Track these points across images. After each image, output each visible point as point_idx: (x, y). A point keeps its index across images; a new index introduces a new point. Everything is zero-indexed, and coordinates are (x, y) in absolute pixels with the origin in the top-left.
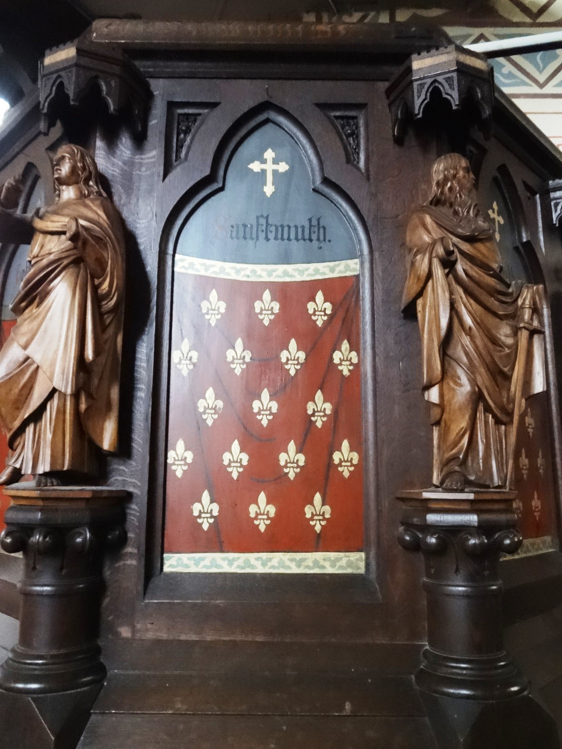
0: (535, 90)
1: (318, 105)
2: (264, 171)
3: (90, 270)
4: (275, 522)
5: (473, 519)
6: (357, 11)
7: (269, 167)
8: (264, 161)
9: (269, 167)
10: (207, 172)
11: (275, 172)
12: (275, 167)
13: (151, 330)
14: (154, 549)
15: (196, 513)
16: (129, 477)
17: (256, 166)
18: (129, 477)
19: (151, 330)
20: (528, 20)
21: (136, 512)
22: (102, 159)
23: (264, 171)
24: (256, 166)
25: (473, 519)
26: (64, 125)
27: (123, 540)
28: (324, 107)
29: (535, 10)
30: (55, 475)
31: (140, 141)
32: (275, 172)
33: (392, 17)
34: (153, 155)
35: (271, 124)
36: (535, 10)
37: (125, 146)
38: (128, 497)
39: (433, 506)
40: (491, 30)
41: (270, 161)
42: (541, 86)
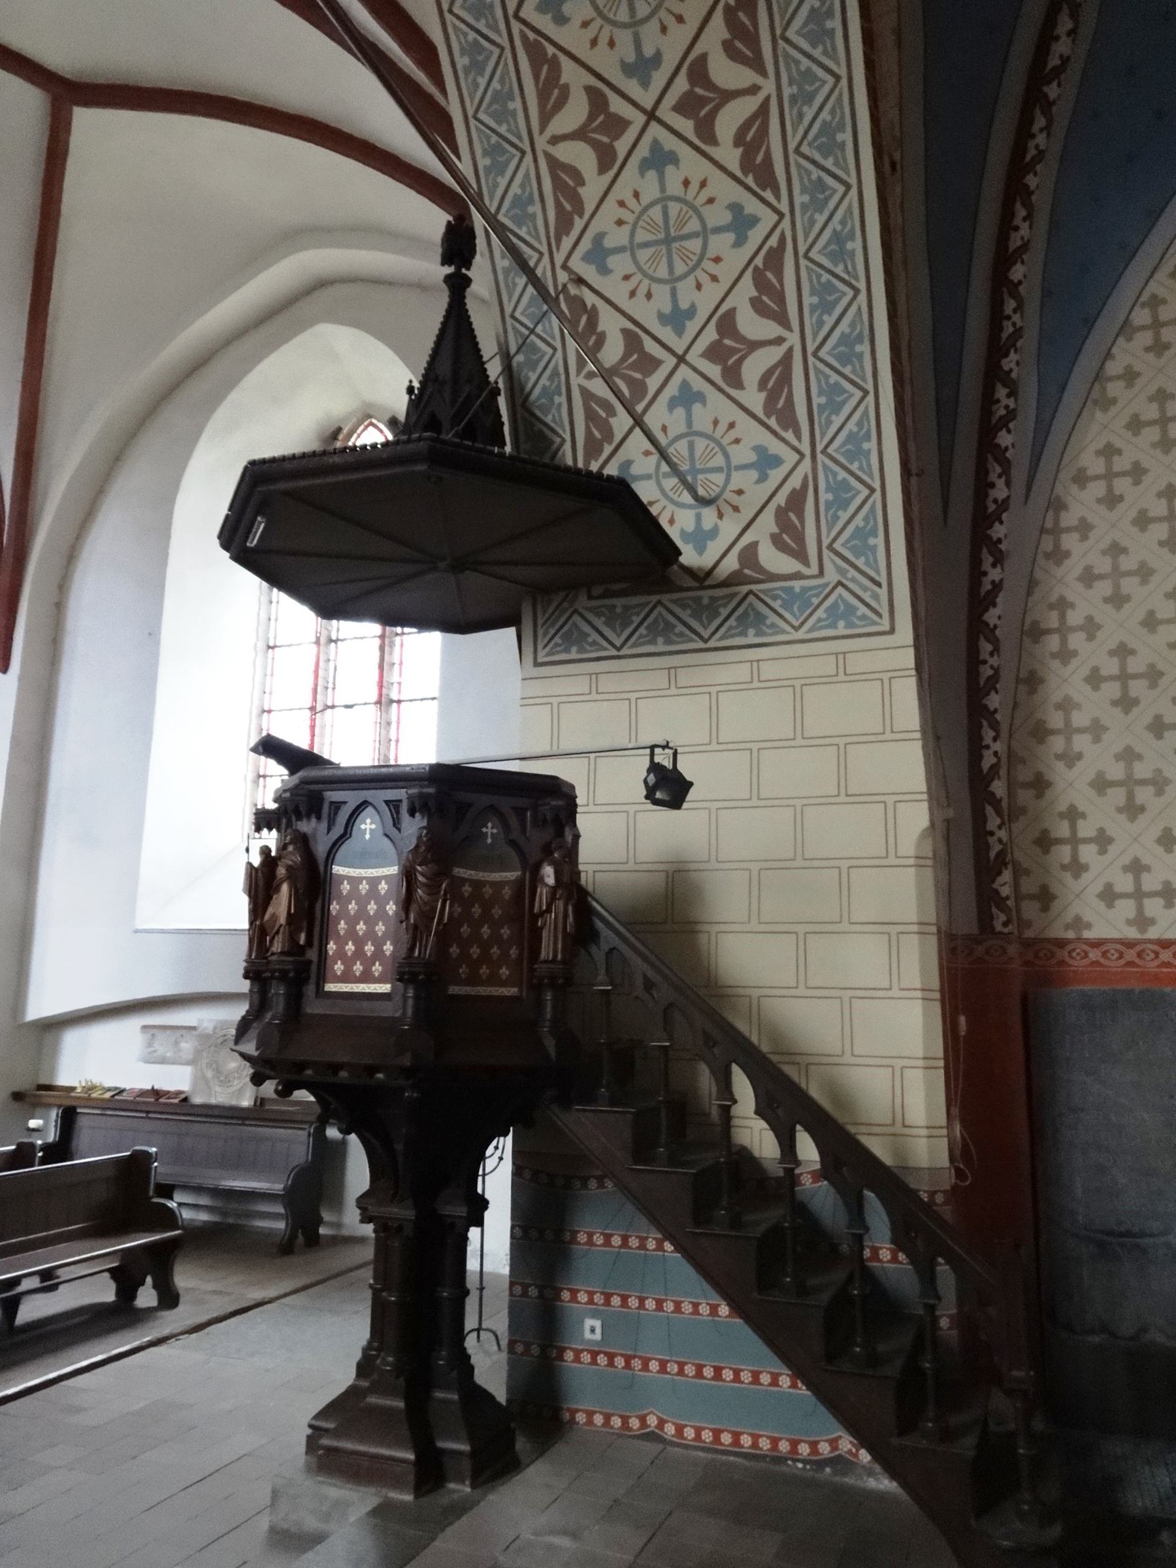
0: (702, 645)
3: (552, 1533)
10: (342, 831)
13: (320, 901)
14: (321, 979)
16: (312, 955)
18: (312, 955)
19: (320, 901)
21: (314, 968)
22: (291, 848)
26: (278, 809)
27: (309, 978)
30: (282, 953)
31: (319, 818)
34: (324, 825)
36: (702, 575)
37: (314, 820)
38: (310, 962)
40: (668, 596)
42: (706, 641)
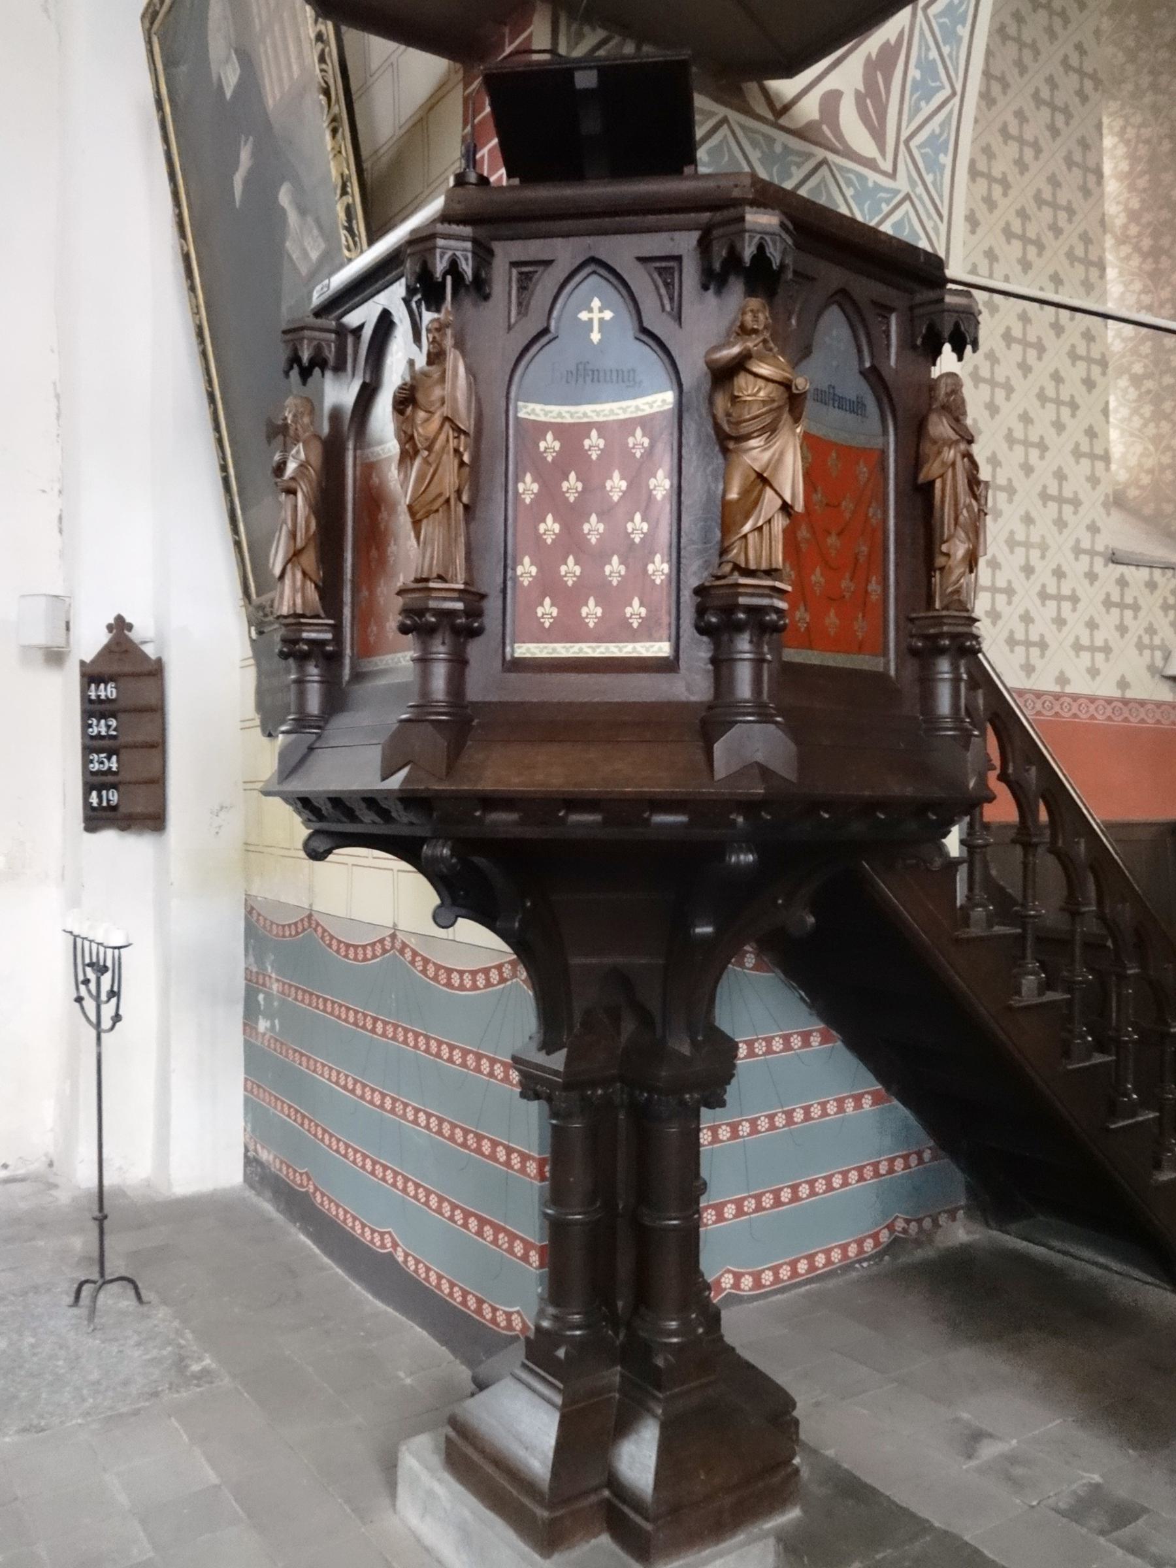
1: (640, 259)
2: (591, 320)
4: (601, 620)
5: (459, 606)
6: (603, 27)
7: (596, 316)
8: (591, 311)
9: (596, 316)
11: (601, 320)
12: (601, 315)
15: (628, 615)
17: (584, 316)
20: (770, 116)
23: (591, 320)
24: (584, 316)
25: (459, 606)
28: (642, 260)
29: (778, 106)
32: (601, 320)
33: (638, 48)
35: (645, 325)
36: (778, 106)
39: (456, 595)
41: (596, 310)
